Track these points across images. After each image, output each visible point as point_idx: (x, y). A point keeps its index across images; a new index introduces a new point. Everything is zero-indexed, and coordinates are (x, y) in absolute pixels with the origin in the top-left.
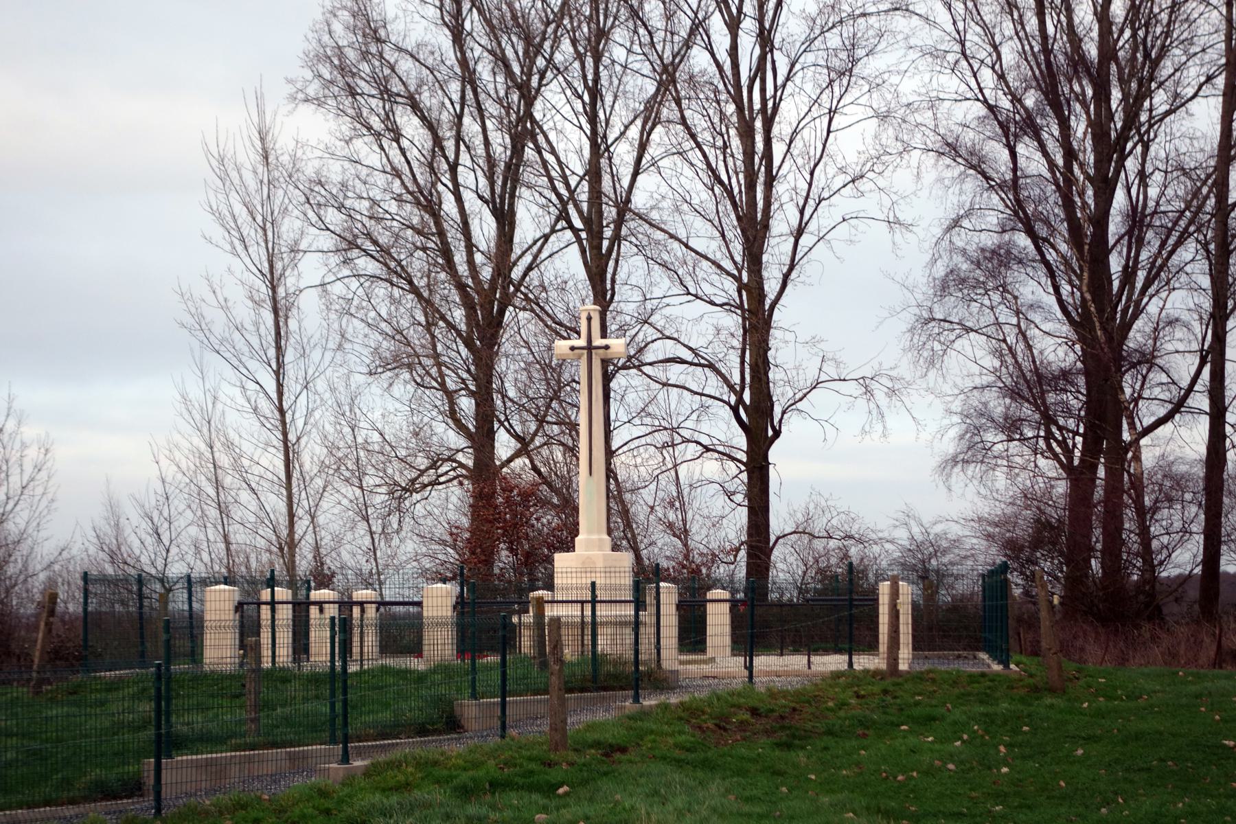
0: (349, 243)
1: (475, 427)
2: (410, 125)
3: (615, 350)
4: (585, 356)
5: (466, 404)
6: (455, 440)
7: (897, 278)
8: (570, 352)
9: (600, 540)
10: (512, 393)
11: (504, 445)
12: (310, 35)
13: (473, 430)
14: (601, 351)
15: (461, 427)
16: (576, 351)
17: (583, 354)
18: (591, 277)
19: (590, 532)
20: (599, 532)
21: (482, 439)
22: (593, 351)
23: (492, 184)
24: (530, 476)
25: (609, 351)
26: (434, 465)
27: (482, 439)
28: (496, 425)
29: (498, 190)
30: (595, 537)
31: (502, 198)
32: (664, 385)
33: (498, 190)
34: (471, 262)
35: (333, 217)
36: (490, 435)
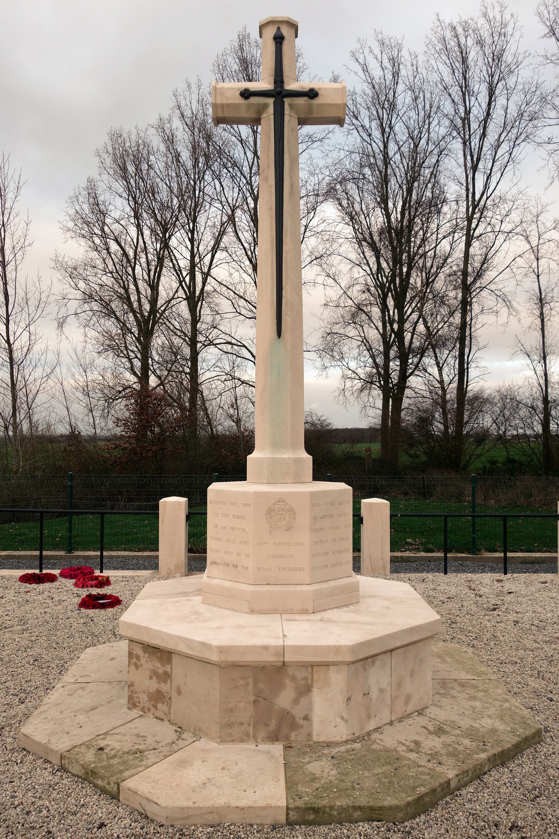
0: (89, 297)
1: (141, 374)
2: (114, 247)
3: (329, 101)
4: (271, 110)
5: (137, 364)
6: (133, 379)
7: (318, 316)
8: (241, 101)
9: (298, 461)
10: (156, 358)
11: (153, 381)
12: (68, 200)
13: (140, 375)
14: (301, 101)
15: (135, 374)
16: (254, 100)
17: (266, 106)
18: (190, 311)
19: (276, 445)
20: (294, 447)
21: (144, 378)
22: (287, 101)
23: (149, 275)
24: (162, 392)
25: (316, 101)
26: (124, 390)
27: (144, 378)
28: (150, 373)
29: (152, 277)
30: (287, 455)
31: (153, 282)
32: (226, 353)
33: (152, 277)
34: (139, 301)
35: (82, 285)
36: (148, 377)
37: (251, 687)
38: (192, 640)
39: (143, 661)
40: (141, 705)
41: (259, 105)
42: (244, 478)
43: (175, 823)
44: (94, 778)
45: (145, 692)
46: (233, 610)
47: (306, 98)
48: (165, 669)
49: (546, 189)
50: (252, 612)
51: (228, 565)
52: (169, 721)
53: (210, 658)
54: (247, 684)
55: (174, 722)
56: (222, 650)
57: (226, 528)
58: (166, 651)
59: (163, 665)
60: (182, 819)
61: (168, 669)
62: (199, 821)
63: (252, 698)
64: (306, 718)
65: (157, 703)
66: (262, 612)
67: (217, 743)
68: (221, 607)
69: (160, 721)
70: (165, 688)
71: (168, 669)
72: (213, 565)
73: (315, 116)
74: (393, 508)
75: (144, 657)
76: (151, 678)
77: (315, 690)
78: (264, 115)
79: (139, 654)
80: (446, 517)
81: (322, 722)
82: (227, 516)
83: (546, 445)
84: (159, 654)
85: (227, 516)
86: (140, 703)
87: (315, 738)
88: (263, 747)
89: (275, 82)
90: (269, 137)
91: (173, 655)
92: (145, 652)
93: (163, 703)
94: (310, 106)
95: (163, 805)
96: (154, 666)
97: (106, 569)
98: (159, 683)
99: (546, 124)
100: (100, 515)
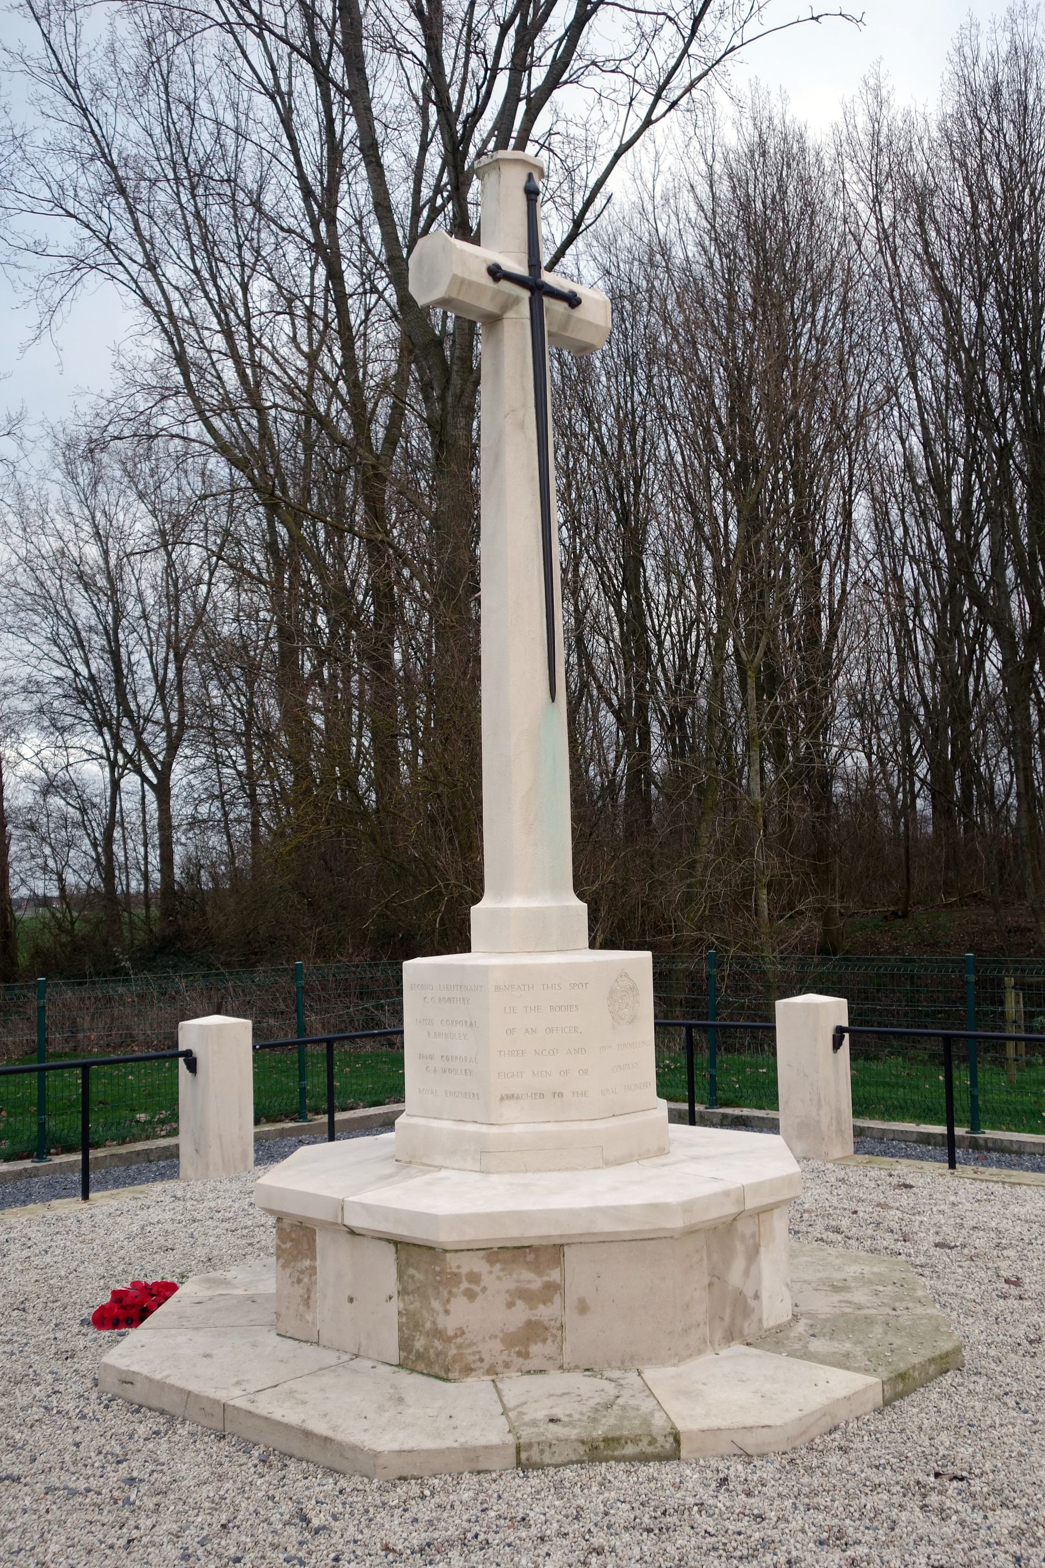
16: (505, 286)
17: (517, 300)
37: (705, 1263)
38: (626, 1208)
39: (487, 1280)
40: (486, 1365)
41: (510, 295)
42: (466, 948)
43: (797, 1443)
44: (615, 1449)
45: (496, 1337)
46: (567, 1169)
47: (565, 305)
48: (546, 1279)
49: (23, 350)
50: (607, 1163)
51: (542, 1096)
52: (561, 1367)
53: (669, 1226)
54: (701, 1260)
55: (572, 1365)
56: (687, 1207)
57: (534, 1031)
58: (546, 1247)
59: (539, 1272)
60: (802, 1434)
61: (555, 1275)
62: (815, 1431)
63: (706, 1281)
64: (757, 1296)
65: (528, 1346)
66: (618, 1162)
67: (674, 1365)
68: (539, 1171)
69: (540, 1376)
70: (544, 1312)
71: (555, 1275)
72: (506, 1102)
73: (568, 334)
74: (256, 1033)
75: (490, 1272)
76: (510, 1305)
77: (762, 1250)
78: (510, 314)
79: (475, 1270)
80: (329, 1042)
81: (770, 1297)
82: (537, 1008)
83: (167, 912)
84: (531, 1257)
85: (537, 1008)
86: (481, 1360)
87: (766, 1325)
88: (724, 1352)
89: (530, 266)
90: (524, 357)
91: (566, 1248)
92: (491, 1262)
93: (545, 1341)
94: (569, 317)
95: (778, 1423)
96: (518, 1281)
97: (104, 1185)
98: (532, 1308)
99: (24, 207)
100: (79, 1071)
